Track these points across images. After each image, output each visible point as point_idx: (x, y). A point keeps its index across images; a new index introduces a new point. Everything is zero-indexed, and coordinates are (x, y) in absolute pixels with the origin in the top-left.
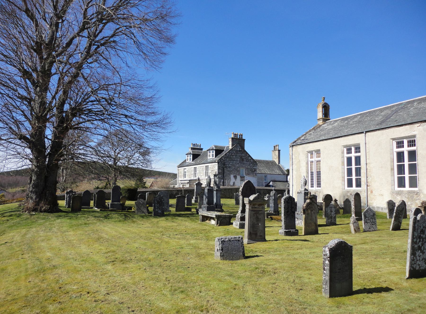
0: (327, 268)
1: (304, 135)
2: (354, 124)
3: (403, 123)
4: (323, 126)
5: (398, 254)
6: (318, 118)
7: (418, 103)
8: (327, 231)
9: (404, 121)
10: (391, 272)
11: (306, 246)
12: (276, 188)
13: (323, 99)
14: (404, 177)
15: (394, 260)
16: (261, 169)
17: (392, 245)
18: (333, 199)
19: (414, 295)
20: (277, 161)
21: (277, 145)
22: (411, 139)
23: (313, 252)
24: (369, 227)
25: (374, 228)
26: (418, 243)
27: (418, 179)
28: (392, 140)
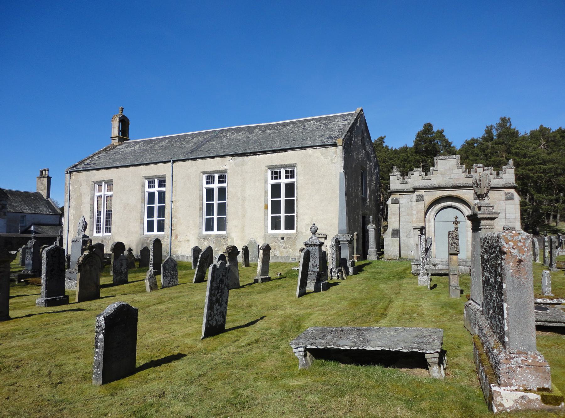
1: (90, 157)
2: (160, 149)
3: (215, 154)
4: (119, 147)
5: (197, 311)
6: (113, 136)
7: (232, 133)
8: (113, 293)
9: (216, 152)
10: (186, 334)
11: (78, 317)
12: (37, 235)
13: (121, 110)
14: (213, 218)
15: (192, 318)
16: (15, 205)
17: (192, 300)
18: (127, 248)
19: (207, 356)
20: (44, 194)
21: (46, 168)
22: (222, 174)
23: (87, 325)
24: (168, 282)
25: (174, 282)
27: (227, 220)
28: (267, 168)
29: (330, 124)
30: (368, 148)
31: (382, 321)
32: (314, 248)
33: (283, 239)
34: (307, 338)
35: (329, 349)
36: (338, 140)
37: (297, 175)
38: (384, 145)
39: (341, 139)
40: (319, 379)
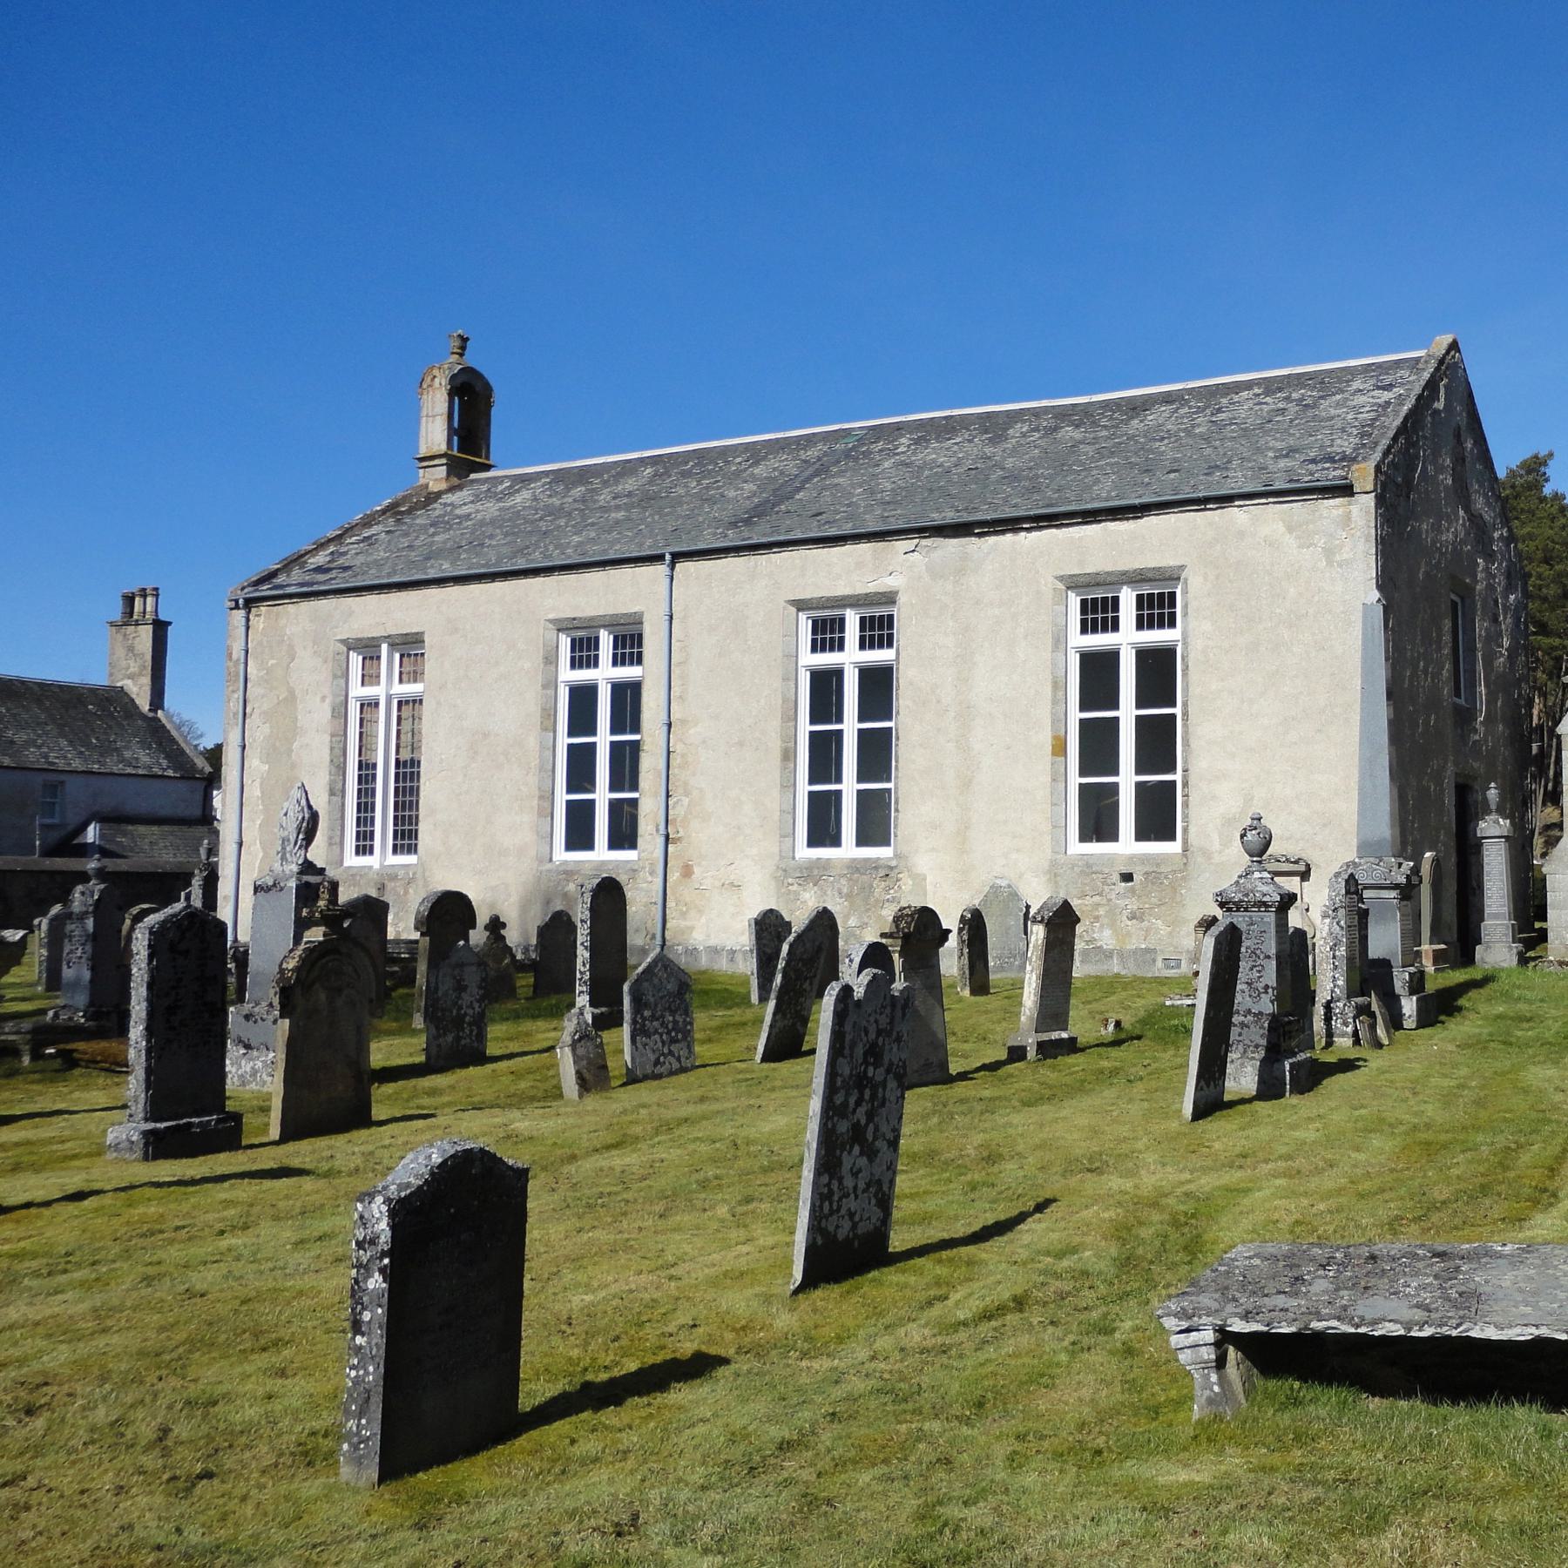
0: (374, 1315)
1: (330, 541)
2: (618, 508)
3: (847, 529)
4: (449, 498)
6: (423, 452)
7: (917, 442)
8: (426, 1101)
10: (726, 1274)
12: (112, 865)
13: (457, 343)
15: (751, 1207)
16: (20, 737)
17: (752, 1133)
18: (482, 918)
19: (816, 1365)
20: (140, 692)
21: (149, 586)
22: (878, 611)
23: (316, 1234)
24: (652, 1057)
25: (679, 1059)
26: (854, 1111)
27: (897, 802)
29: (1324, 403)
30: (1479, 503)
31: (1539, 1218)
32: (1256, 915)
33: (1127, 877)
34: (1227, 1288)
35: (1319, 1336)
36: (1354, 467)
37: (1185, 615)
38: (1548, 490)
39: (1369, 467)
40: (1276, 1459)
